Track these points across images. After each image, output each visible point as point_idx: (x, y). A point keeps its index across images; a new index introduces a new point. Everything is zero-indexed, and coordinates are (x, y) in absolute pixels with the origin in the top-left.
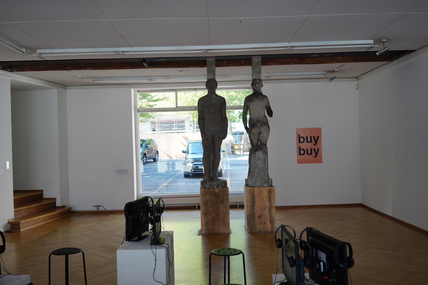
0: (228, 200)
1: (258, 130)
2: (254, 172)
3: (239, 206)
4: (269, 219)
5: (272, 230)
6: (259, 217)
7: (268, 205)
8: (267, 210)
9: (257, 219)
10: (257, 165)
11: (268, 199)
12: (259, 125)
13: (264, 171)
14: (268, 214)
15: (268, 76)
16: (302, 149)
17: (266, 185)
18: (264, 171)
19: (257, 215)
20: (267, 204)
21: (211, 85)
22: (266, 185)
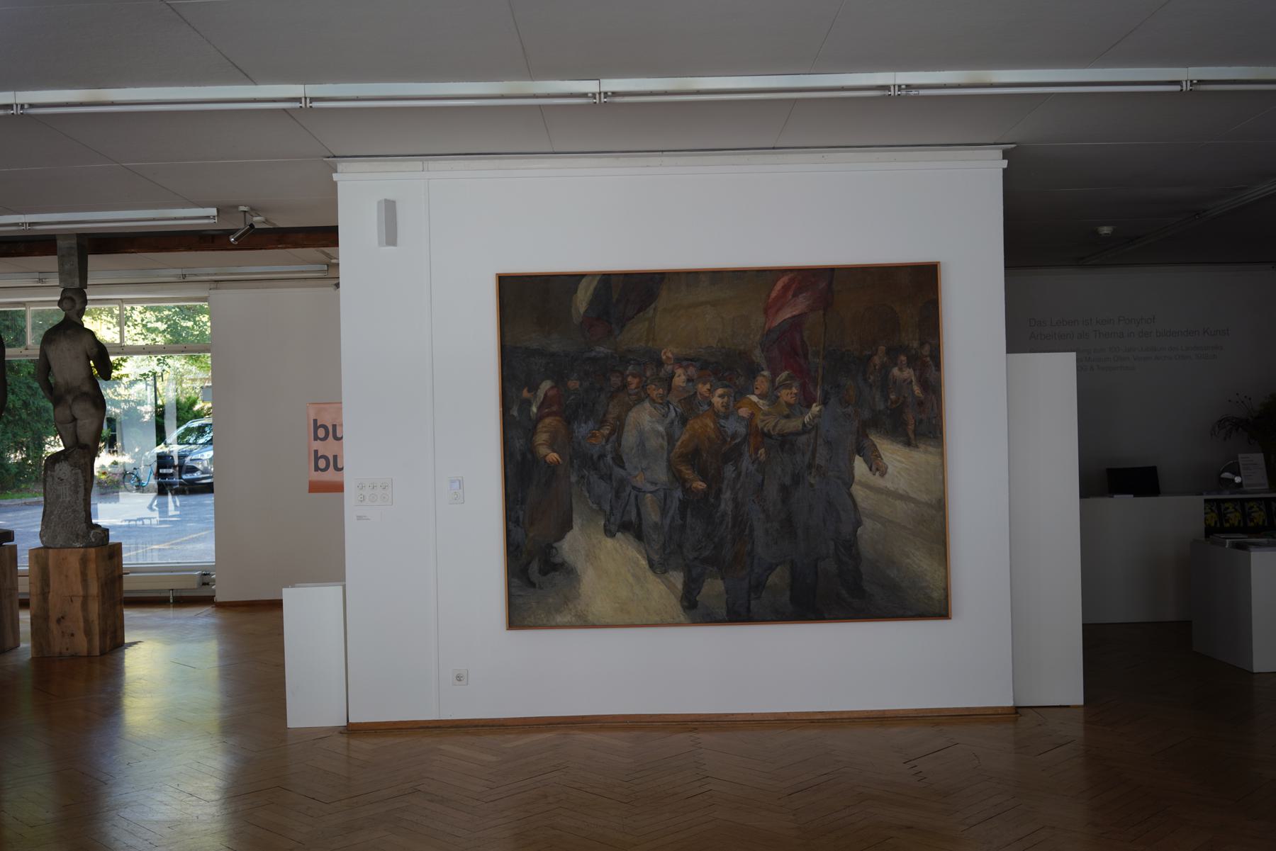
0: (17, 589)
1: (68, 412)
2: (52, 512)
3: (25, 604)
4: (82, 624)
5: (89, 651)
6: (59, 621)
7: (81, 593)
8: (78, 603)
9: (53, 625)
10: (58, 497)
11: (79, 579)
12: (69, 398)
13: (74, 511)
14: (80, 614)
15: (184, 276)
16: (323, 457)
17: (77, 545)
18: (74, 511)
19: (54, 614)
20: (78, 589)
21: (75, 300)
22: (77, 545)
